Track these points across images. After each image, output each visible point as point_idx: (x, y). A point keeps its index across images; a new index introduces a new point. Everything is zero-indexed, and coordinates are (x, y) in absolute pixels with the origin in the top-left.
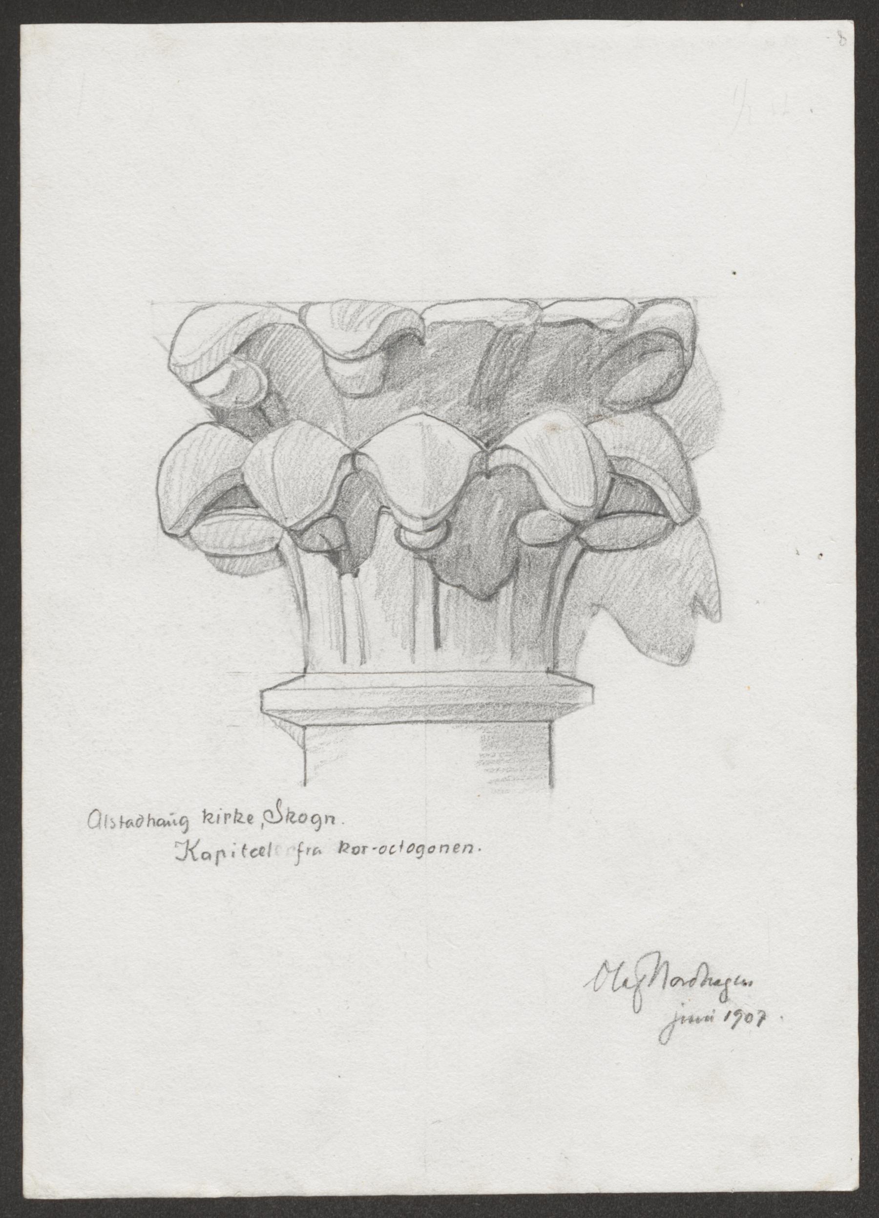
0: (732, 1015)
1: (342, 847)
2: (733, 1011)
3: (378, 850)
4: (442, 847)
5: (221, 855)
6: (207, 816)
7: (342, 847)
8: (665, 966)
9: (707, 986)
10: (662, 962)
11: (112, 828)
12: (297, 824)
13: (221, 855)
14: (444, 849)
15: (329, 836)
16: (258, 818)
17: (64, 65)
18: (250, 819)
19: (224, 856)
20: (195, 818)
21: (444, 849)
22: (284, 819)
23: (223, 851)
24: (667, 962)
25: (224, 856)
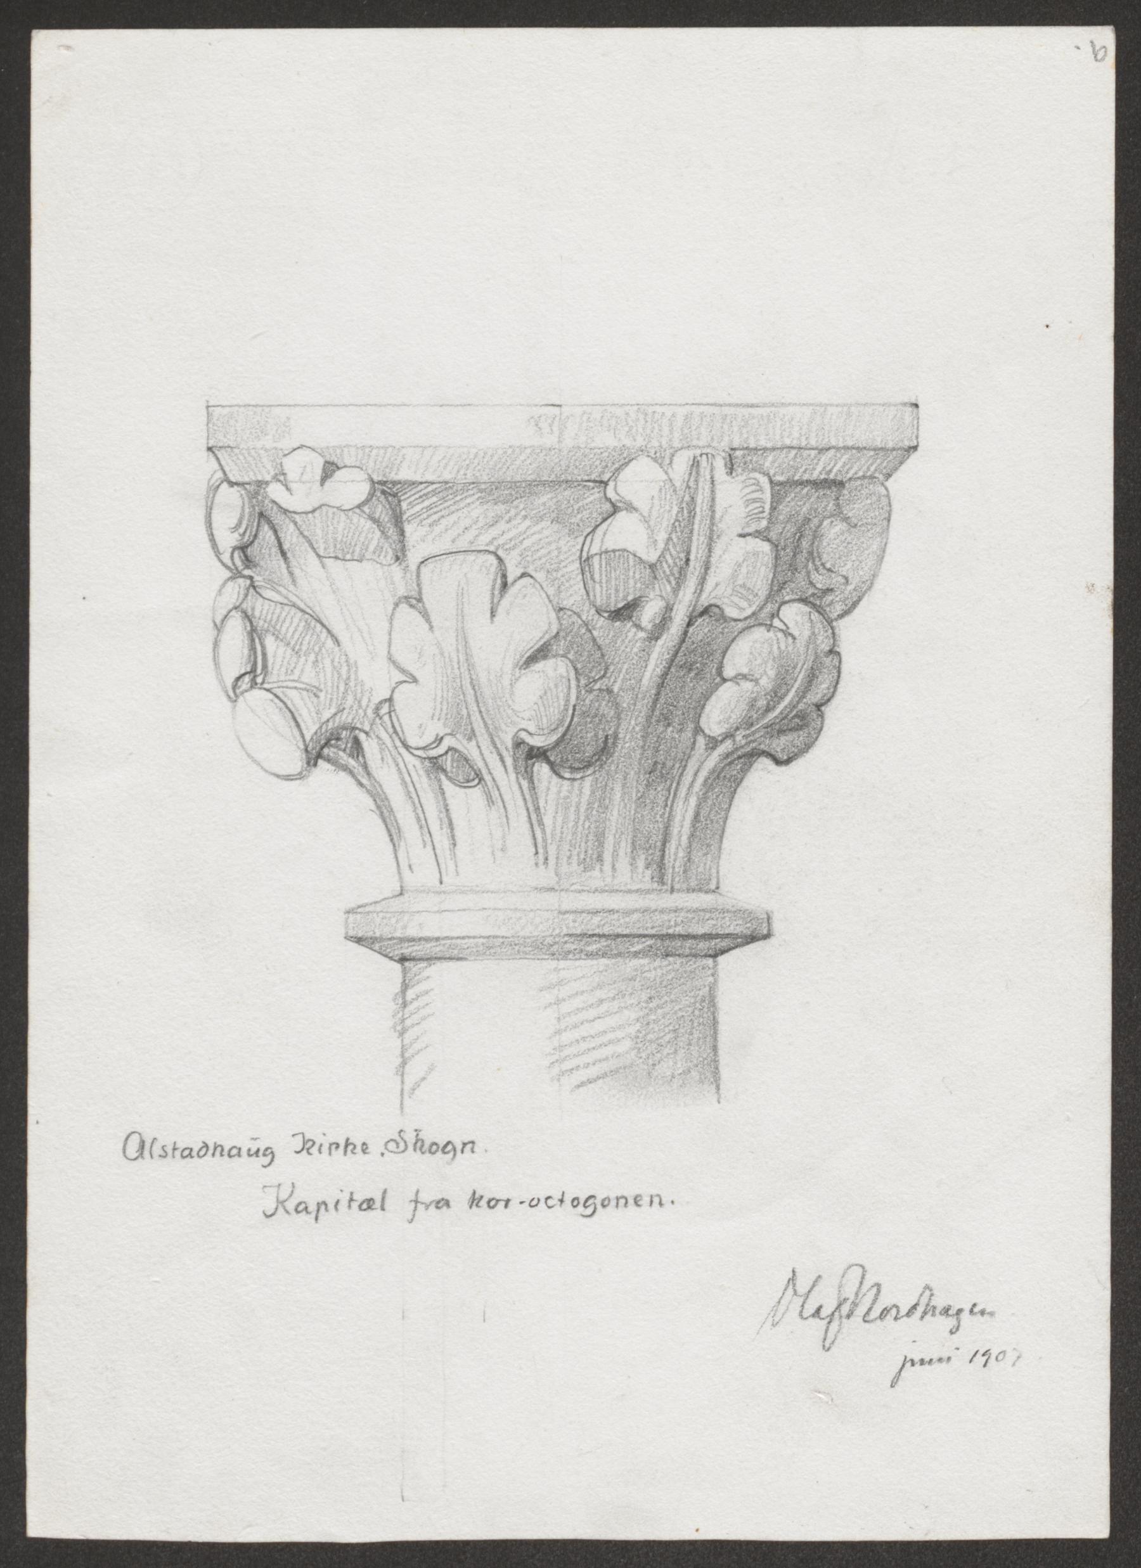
0: (979, 1355)
1: (475, 1200)
2: (982, 1352)
3: (527, 1204)
4: (465, 1144)
5: (323, 1207)
6: (307, 1146)
7: (475, 1200)
8: (875, 1290)
9: (928, 1317)
10: (868, 1283)
11: (549, 1198)
12: (428, 1155)
13: (323, 1207)
14: (622, 1201)
15: (459, 1177)
16: (375, 1148)
17: (84, 83)
18: (365, 1148)
19: (326, 1210)
20: (286, 1146)
21: (622, 1201)
22: (411, 1147)
23: (325, 1203)
24: (878, 1286)
25: (326, 1210)
